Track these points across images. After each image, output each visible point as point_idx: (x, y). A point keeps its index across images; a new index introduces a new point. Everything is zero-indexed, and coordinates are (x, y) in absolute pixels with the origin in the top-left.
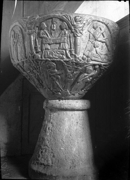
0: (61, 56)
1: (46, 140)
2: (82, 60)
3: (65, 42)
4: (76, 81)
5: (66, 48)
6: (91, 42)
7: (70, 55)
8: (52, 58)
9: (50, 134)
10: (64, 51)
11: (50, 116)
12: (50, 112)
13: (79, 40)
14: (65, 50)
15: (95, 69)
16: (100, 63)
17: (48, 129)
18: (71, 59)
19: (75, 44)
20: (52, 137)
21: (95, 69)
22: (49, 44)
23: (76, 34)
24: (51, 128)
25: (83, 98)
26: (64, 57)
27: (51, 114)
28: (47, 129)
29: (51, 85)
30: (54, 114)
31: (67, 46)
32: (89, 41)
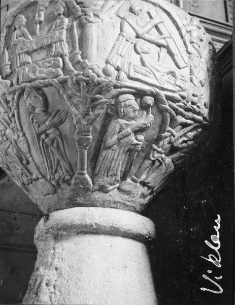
0: (54, 70)
2: (103, 75)
3: (61, 41)
4: (100, 145)
5: (62, 49)
6: (125, 39)
7: (73, 66)
8: (35, 80)
9: (50, 297)
10: (61, 60)
11: (52, 251)
13: (94, 31)
14: (62, 56)
15: (144, 107)
16: (158, 90)
18: (76, 72)
19: (83, 41)
21: (144, 107)
22: (29, 53)
23: (86, 19)
24: (53, 283)
25: (145, 211)
26: (61, 72)
27: (58, 245)
28: (44, 284)
29: (45, 164)
30: (65, 245)
31: (66, 50)
32: (120, 35)
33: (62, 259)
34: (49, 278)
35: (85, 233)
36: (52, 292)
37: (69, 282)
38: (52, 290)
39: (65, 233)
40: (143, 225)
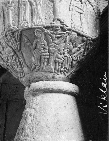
1: (27, 129)
9: (32, 121)
11: (32, 101)
12: (32, 97)
17: (30, 116)
20: (34, 124)
24: (33, 115)
25: (72, 80)
27: (34, 98)
28: (29, 115)
33: (36, 104)
34: (31, 113)
35: (46, 92)
36: (32, 119)
37: (40, 114)
38: (32, 118)
39: (37, 93)
40: (72, 87)
